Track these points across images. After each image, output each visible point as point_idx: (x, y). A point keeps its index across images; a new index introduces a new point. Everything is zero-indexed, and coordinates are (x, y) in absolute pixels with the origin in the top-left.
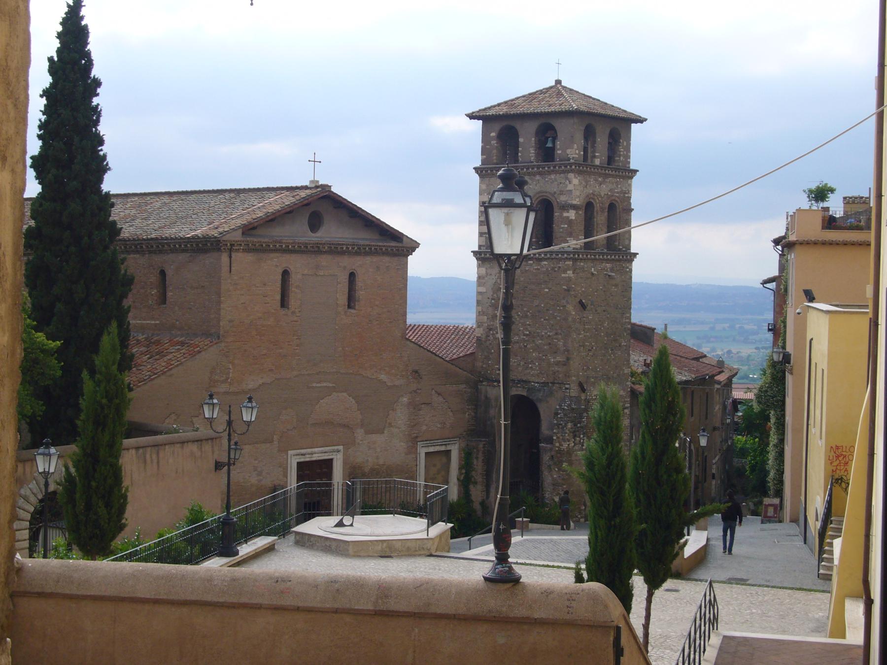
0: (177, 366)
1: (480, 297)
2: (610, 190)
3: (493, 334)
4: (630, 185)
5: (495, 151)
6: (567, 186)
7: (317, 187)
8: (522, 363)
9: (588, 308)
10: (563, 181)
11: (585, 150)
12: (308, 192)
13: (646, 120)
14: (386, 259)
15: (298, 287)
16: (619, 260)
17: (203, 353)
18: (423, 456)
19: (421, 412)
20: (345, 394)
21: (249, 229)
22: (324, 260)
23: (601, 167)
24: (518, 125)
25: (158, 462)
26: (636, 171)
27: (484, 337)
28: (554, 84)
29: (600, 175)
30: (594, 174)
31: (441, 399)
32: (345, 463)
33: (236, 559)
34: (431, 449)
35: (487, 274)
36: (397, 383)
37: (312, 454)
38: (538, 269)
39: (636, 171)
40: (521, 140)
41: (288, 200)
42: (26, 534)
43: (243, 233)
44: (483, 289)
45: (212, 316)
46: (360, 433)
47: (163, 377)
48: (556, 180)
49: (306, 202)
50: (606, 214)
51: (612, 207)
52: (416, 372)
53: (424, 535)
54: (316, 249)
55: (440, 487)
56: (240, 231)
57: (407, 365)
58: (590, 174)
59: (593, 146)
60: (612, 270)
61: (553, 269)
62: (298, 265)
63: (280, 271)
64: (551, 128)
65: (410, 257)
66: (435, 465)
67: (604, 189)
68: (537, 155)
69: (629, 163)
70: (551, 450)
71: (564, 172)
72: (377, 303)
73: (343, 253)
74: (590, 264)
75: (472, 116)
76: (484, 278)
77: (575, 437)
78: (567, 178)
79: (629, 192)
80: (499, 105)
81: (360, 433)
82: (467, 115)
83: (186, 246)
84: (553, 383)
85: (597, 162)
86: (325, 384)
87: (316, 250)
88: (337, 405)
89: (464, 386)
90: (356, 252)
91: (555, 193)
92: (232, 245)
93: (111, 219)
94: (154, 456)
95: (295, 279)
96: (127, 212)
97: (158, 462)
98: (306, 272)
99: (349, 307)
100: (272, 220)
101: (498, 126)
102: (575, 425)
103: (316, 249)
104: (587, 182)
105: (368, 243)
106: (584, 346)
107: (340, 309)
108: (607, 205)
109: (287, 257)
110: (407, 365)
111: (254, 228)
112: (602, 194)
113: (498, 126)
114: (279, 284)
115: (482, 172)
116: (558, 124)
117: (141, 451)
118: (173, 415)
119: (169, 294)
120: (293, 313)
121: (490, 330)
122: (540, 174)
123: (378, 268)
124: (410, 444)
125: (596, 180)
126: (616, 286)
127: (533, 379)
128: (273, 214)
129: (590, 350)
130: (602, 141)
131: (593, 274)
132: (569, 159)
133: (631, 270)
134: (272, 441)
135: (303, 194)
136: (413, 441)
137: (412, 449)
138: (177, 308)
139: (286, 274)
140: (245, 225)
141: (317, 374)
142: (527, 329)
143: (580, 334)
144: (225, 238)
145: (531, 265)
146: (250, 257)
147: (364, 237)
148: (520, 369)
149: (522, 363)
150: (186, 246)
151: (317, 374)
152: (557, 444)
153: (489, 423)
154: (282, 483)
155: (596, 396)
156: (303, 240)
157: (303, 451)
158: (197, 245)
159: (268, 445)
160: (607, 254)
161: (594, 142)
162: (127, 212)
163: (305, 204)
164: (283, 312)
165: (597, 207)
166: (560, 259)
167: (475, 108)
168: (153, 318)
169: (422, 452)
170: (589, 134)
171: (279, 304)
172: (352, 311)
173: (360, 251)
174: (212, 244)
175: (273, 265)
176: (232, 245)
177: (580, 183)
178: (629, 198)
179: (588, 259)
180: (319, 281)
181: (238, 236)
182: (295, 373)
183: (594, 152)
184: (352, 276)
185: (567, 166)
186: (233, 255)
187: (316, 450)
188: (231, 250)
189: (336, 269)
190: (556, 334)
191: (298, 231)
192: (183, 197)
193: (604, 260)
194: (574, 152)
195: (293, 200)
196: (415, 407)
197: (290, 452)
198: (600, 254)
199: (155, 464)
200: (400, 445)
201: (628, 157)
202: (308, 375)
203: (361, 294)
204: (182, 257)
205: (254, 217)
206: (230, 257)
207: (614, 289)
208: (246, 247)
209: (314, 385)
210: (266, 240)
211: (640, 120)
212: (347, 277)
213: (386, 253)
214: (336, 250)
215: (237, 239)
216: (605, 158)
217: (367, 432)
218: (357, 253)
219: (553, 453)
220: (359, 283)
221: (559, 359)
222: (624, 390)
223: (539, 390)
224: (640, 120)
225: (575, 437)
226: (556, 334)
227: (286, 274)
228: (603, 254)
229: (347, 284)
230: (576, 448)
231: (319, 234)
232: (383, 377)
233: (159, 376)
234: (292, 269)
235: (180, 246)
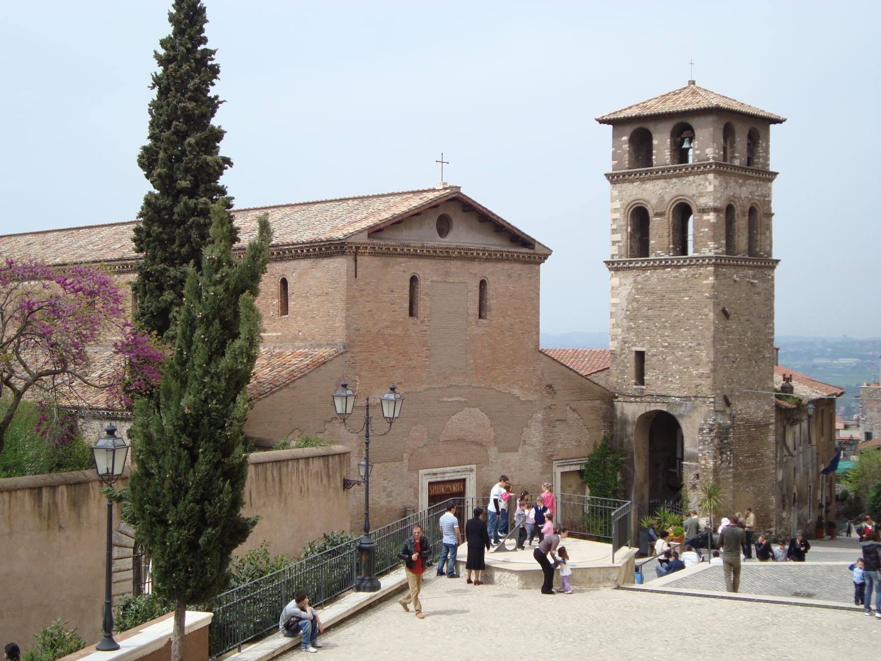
0: (300, 378)
1: (613, 309)
2: (751, 193)
3: (628, 347)
4: (770, 188)
5: (627, 156)
6: (706, 187)
7: (445, 189)
8: (661, 377)
9: (731, 317)
10: (702, 182)
11: (725, 149)
12: (437, 194)
13: (785, 120)
14: (518, 267)
15: (427, 294)
16: (761, 267)
17: (328, 364)
18: (559, 476)
19: (556, 430)
20: (477, 410)
21: (375, 231)
22: (454, 266)
23: (742, 169)
24: (651, 127)
25: (280, 480)
26: (775, 174)
27: (618, 350)
28: (687, 85)
29: (741, 176)
30: (735, 175)
31: (576, 416)
32: (478, 483)
33: (378, 594)
34: (567, 469)
35: (621, 284)
36: (531, 398)
37: (444, 473)
38: (677, 277)
39: (775, 174)
40: (655, 142)
41: (415, 202)
42: (129, 563)
43: (369, 236)
44: (616, 300)
45: (337, 325)
46: (493, 451)
47: (285, 390)
48: (694, 181)
49: (434, 204)
50: (747, 218)
51: (752, 211)
52: (550, 386)
53: (609, 563)
54: (446, 254)
55: (624, 503)
56: (366, 233)
57: (541, 380)
58: (730, 175)
59: (732, 147)
60: (754, 277)
61: (693, 275)
62: (426, 270)
63: (409, 277)
64: (690, 129)
65: (542, 265)
66: (570, 486)
67: (744, 191)
68: (672, 157)
69: (768, 165)
70: (696, 468)
71: (703, 173)
72: (510, 312)
73: (473, 259)
74: (733, 270)
75: (602, 121)
76: (617, 288)
77: (721, 453)
78: (706, 179)
79: (769, 195)
80: (630, 108)
81: (493, 451)
82: (597, 120)
83: (308, 251)
84: (696, 397)
85: (737, 163)
86: (456, 399)
87: (446, 255)
88: (470, 421)
89: (599, 402)
90: (486, 258)
91: (694, 195)
92: (357, 248)
93: (218, 144)
94: (275, 473)
95: (423, 285)
96: (247, 224)
97: (280, 480)
98: (435, 279)
99: (480, 317)
100: (399, 222)
101: (629, 130)
102: (722, 441)
103: (446, 254)
104: (727, 183)
105: (499, 248)
106: (727, 357)
107: (471, 319)
108: (748, 209)
109: (416, 262)
110: (541, 380)
111: (380, 230)
112: (743, 197)
113: (629, 130)
114: (407, 291)
115: (613, 177)
116: (694, 122)
117: (260, 467)
118: (296, 431)
119: (291, 304)
120: (423, 322)
121: (625, 343)
122: (677, 176)
123: (509, 276)
124: (545, 463)
125: (736, 182)
126: (759, 293)
127: (673, 393)
128: (400, 215)
129: (734, 362)
130: (741, 141)
131: (735, 281)
132: (708, 159)
133: (773, 278)
134: (401, 460)
135: (431, 196)
136: (549, 459)
137: (547, 469)
138: (299, 318)
139: (414, 280)
140: (371, 228)
141: (448, 387)
142: (665, 341)
143: (723, 345)
144: (350, 240)
145: (669, 272)
146: (376, 262)
147: (495, 244)
148: (659, 383)
149: (661, 377)
150: (308, 251)
151: (448, 387)
152: (703, 462)
153: (625, 440)
154: (413, 505)
155: (741, 410)
156: (432, 244)
157: (434, 470)
158: (320, 249)
159: (398, 464)
160: (750, 260)
161: (733, 142)
162: (247, 224)
163: (433, 206)
164: (411, 320)
165: (738, 210)
166: (702, 265)
167: (606, 112)
168: (275, 330)
169: (558, 471)
170: (728, 133)
171: (407, 313)
172: (483, 321)
173: (491, 257)
174: (336, 248)
175: (400, 271)
176: (357, 248)
177: (721, 185)
178: (770, 202)
179: (730, 265)
180: (449, 289)
181: (364, 238)
182: (425, 386)
183: (733, 152)
184: (483, 283)
185: (701, 169)
186: (359, 258)
187: (448, 469)
188: (356, 254)
189: (467, 276)
190: (699, 344)
191: (426, 235)
192: (304, 207)
193: (746, 266)
194: (711, 153)
195: (422, 202)
196: (549, 424)
197: (421, 472)
198: (742, 259)
199: (277, 482)
200: (535, 464)
201: (767, 159)
202: (439, 388)
203: (492, 302)
204: (304, 264)
205: (380, 218)
206: (356, 261)
207: (756, 297)
208: (372, 251)
209: (445, 399)
210: (393, 243)
211: (778, 121)
212: (478, 284)
213: (517, 260)
214: (466, 256)
215: (363, 241)
216: (744, 159)
217: (501, 450)
218: (488, 260)
219: (699, 471)
220: (490, 291)
221: (701, 371)
222: (768, 404)
223: (680, 405)
224: (778, 121)
225: (721, 453)
226: (699, 344)
227: (414, 280)
228: (746, 260)
229: (478, 292)
230: (723, 465)
231: (447, 239)
232: (516, 392)
233: (281, 389)
234: (420, 275)
235: (302, 251)
